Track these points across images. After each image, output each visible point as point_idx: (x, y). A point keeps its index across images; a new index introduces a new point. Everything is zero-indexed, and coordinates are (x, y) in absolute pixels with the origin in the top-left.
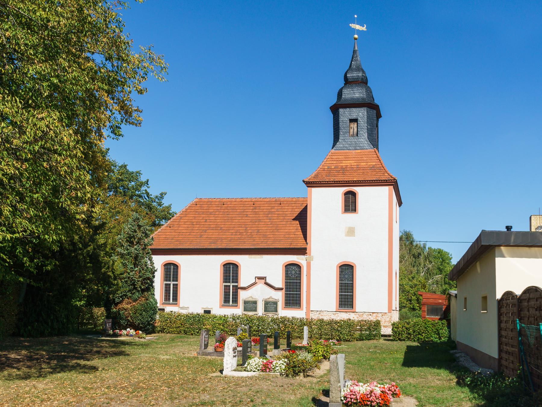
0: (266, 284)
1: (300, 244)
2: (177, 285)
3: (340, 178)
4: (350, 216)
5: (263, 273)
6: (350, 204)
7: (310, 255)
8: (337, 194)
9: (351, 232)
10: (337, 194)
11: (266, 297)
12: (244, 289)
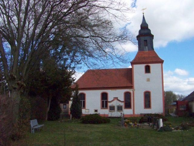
0: (118, 100)
1: (130, 85)
3: (144, 61)
4: (148, 74)
5: (116, 95)
6: (148, 70)
7: (134, 89)
8: (142, 67)
9: (148, 80)
10: (142, 67)
11: (118, 105)
12: (110, 102)
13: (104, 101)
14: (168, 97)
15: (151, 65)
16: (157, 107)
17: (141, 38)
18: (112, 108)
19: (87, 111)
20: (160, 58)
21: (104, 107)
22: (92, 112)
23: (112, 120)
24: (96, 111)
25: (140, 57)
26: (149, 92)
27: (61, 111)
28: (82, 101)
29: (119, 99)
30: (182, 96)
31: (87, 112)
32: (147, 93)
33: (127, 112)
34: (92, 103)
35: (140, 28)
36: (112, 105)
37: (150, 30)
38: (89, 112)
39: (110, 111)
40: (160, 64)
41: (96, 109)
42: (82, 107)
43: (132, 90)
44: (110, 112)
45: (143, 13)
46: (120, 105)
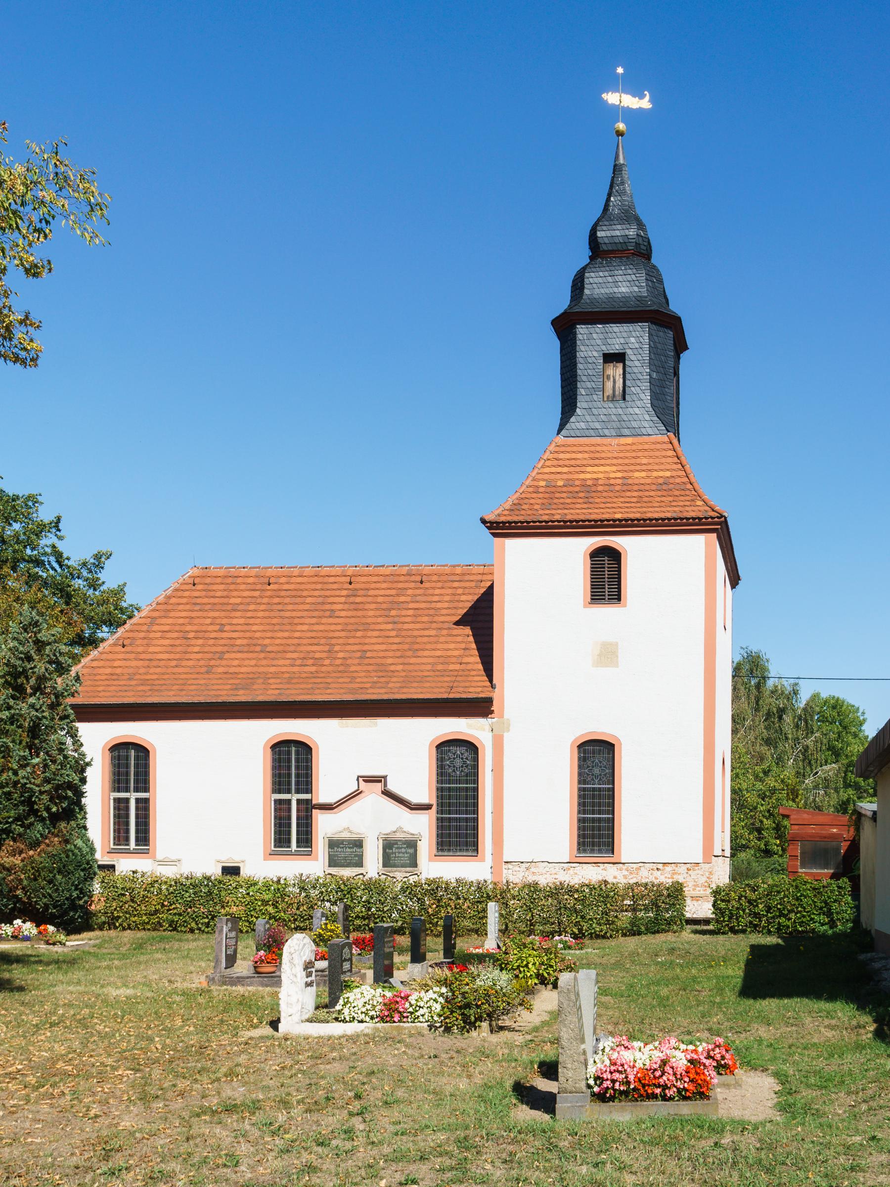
0: (387, 794)
1: (476, 688)
2: (146, 801)
4: (606, 612)
5: (371, 767)
6: (606, 579)
9: (608, 655)
12: (327, 807)
13: (127, 800)
17: (582, 331)
21: (289, 841)
26: (613, 745)
32: (544, 1068)
34: (206, 800)
46: (348, 829)
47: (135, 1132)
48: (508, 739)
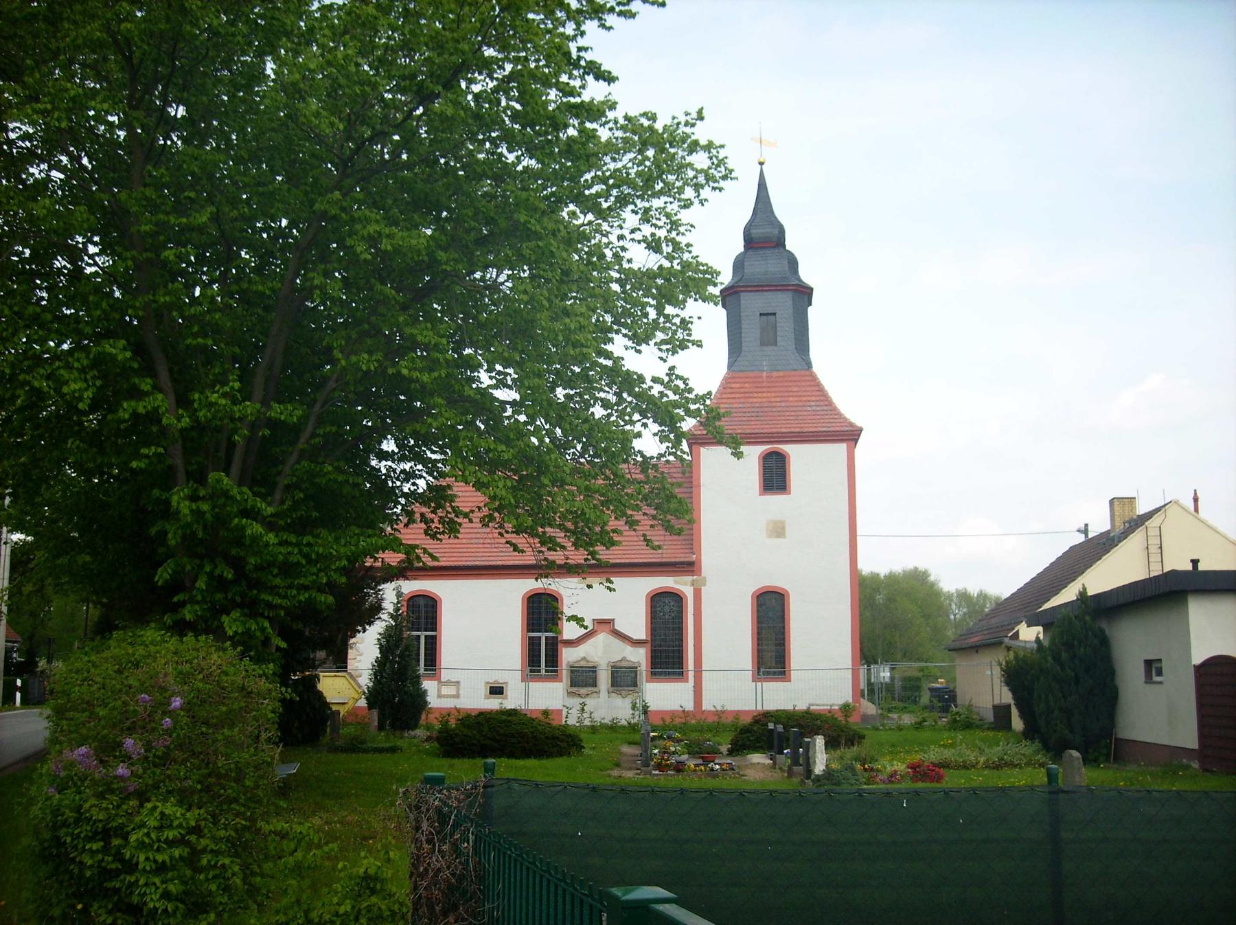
1: (671, 551)
2: (434, 638)
4: (775, 501)
6: (775, 477)
11: (616, 658)
12: (570, 643)
14: (891, 616)
15: (794, 452)
16: (823, 671)
18: (583, 678)
19: (445, 690)
20: (840, 415)
22: (475, 700)
23: (588, 741)
24: (497, 691)
25: (280, 468)
27: (562, 613)
28: (419, 637)
29: (618, 626)
30: (983, 596)
31: (445, 696)
33: (666, 696)
35: (739, 247)
36: (584, 659)
37: (793, 262)
38: (457, 696)
39: (574, 690)
40: (843, 447)
41: (497, 678)
42: (422, 671)
43: (689, 579)
44: (570, 694)
45: (761, 164)
47: (141, 806)
48: (705, 591)
